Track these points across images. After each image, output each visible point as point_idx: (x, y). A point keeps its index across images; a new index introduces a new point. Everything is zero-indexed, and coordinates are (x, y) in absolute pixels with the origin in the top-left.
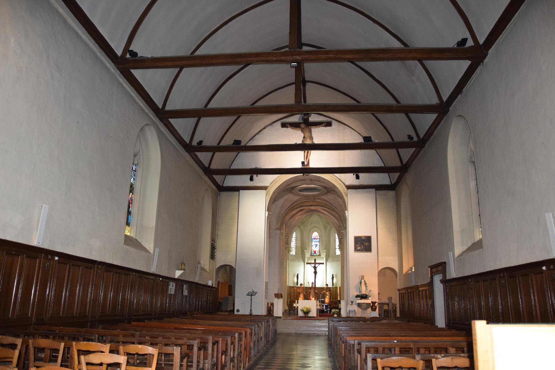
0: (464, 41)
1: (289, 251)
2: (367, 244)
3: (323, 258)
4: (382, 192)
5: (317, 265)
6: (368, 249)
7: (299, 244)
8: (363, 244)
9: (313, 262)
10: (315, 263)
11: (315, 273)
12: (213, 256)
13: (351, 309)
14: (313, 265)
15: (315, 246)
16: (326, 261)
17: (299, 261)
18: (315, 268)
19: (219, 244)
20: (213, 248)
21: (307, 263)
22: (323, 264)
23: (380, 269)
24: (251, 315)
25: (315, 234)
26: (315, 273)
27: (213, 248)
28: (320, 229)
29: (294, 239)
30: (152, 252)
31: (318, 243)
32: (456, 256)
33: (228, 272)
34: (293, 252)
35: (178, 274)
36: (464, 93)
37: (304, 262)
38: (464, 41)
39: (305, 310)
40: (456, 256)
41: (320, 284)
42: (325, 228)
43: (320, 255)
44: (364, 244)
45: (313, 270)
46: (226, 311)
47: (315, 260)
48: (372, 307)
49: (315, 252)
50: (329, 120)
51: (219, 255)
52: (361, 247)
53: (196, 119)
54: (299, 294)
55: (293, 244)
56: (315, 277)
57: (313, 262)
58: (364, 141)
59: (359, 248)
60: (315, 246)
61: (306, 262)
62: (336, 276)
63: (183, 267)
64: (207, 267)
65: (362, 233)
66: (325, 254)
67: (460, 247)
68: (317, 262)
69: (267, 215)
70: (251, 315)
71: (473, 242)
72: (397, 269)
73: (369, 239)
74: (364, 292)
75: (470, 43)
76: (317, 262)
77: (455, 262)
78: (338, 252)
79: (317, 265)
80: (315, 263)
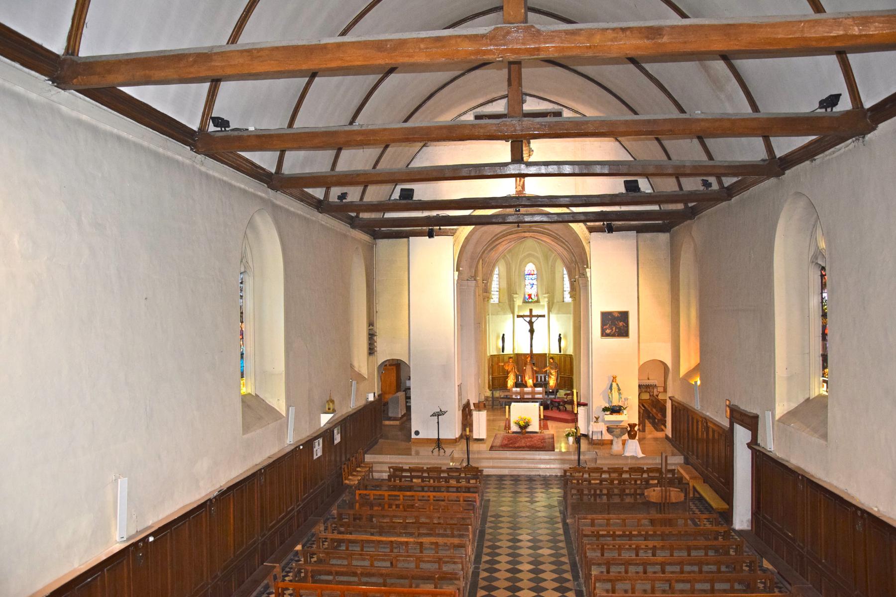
0: (834, 100)
1: (489, 298)
2: (621, 324)
3: (543, 306)
4: (648, 235)
5: (534, 319)
6: (623, 332)
7: (504, 285)
8: (615, 325)
9: (528, 314)
10: (531, 316)
11: (532, 331)
12: (371, 351)
13: (595, 430)
14: (528, 319)
15: (530, 287)
16: (549, 311)
17: (505, 313)
18: (531, 323)
19: (381, 326)
20: (371, 336)
21: (519, 316)
22: (544, 316)
23: (641, 363)
24: (439, 439)
25: (530, 267)
26: (532, 331)
27: (371, 336)
28: (537, 258)
29: (495, 278)
30: (284, 414)
31: (535, 282)
32: (777, 417)
33: (396, 374)
34: (495, 298)
35: (325, 419)
36: (818, 162)
37: (513, 313)
38: (834, 100)
39: (522, 423)
40: (777, 417)
41: (540, 348)
42: (547, 258)
43: (538, 301)
44: (616, 324)
45: (529, 328)
46: (395, 419)
47: (531, 310)
48: (629, 433)
49: (530, 296)
50: (556, 108)
51: (381, 344)
52: (612, 329)
53: (332, 153)
54: (508, 373)
55: (495, 286)
56: (532, 339)
57: (528, 314)
58: (627, 189)
59: (608, 331)
60: (530, 287)
61: (516, 313)
62: (565, 337)
63: (331, 406)
64: (364, 371)
65: (615, 307)
66: (546, 299)
67: (785, 403)
68: (534, 314)
69: (456, 278)
70: (439, 439)
71: (807, 396)
72: (669, 364)
73: (624, 316)
74: (615, 402)
75: (845, 104)
76: (534, 314)
77: (776, 428)
78: (568, 299)
79: (534, 319)
80: (531, 316)
